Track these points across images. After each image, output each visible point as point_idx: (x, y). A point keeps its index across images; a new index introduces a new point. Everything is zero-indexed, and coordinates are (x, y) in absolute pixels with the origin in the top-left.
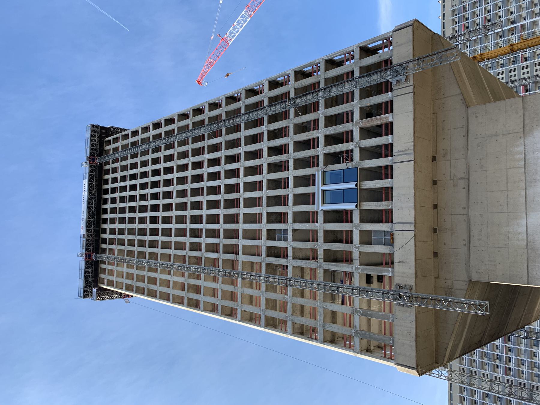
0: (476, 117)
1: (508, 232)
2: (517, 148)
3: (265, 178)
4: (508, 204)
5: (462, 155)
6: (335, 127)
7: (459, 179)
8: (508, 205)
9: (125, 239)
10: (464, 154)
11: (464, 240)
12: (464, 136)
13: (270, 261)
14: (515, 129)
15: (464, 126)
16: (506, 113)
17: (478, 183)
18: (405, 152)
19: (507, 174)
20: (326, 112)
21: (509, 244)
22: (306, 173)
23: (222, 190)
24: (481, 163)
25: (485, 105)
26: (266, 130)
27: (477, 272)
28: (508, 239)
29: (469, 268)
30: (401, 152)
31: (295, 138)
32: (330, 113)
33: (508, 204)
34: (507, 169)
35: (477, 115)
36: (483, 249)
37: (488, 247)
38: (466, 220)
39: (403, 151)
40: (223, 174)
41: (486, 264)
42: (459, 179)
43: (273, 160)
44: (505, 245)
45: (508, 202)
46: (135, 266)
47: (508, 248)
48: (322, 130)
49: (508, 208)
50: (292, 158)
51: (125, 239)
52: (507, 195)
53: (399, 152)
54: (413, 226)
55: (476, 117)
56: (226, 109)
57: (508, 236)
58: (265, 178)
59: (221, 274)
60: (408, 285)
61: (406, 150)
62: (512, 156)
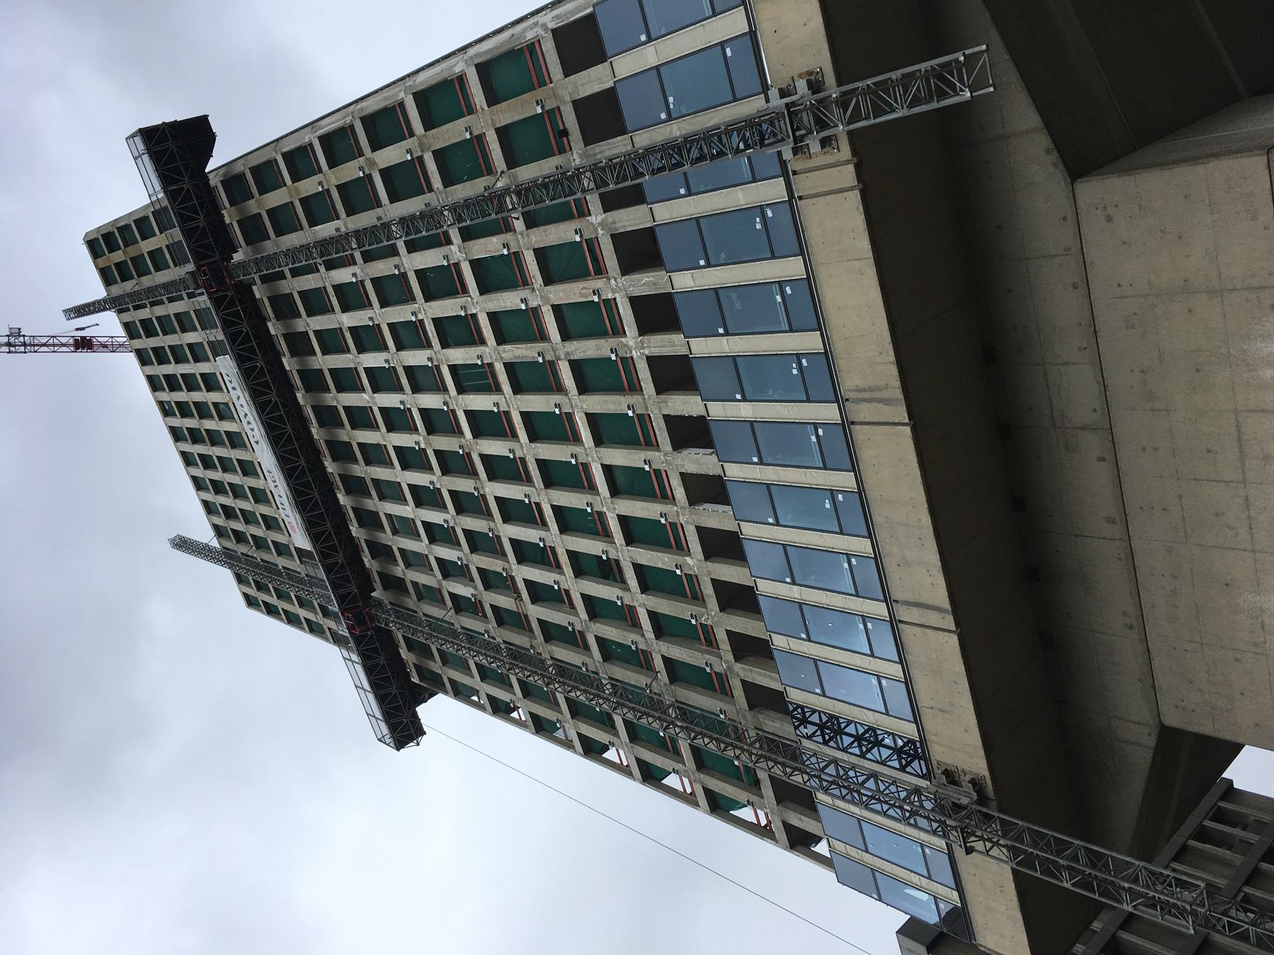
0: (1109, 219)
1: (1261, 609)
2: (1263, 345)
3: (513, 407)
4: (1250, 525)
5: (1080, 349)
6: (652, 276)
7: (1081, 428)
8: (1251, 528)
9: (292, 202)
10: (1085, 349)
11: (1124, 614)
12: (1076, 288)
13: (604, 632)
14: (1253, 275)
15: (1069, 249)
16: (1136, 410)
17: (1144, 449)
18: (877, 395)
19: (1238, 427)
20: (610, 220)
21: (1268, 645)
22: (616, 410)
23: (420, 425)
24: (1145, 385)
25: (1132, 177)
26: (465, 260)
27: (1176, 707)
28: (1263, 629)
29: (1154, 693)
30: (864, 390)
31: (551, 296)
32: (624, 226)
33: (1250, 525)
34: (1236, 412)
35: (1111, 211)
36: (1188, 648)
37: (1201, 644)
38: (1123, 556)
39: (870, 389)
40: (403, 378)
41: (1200, 690)
42: (1081, 428)
43: (515, 357)
44: (1256, 644)
45: (1249, 517)
46: (358, 255)
47: (1266, 655)
48: (619, 280)
49: (1252, 537)
50: (506, 672)
51: (292, 202)
52: (1247, 499)
53: (860, 391)
54: (950, 619)
55: (1109, 219)
56: (336, 177)
57: (1260, 621)
58: (513, 407)
59: (592, 185)
60: (970, 772)
61: (879, 389)
62: (1251, 371)
